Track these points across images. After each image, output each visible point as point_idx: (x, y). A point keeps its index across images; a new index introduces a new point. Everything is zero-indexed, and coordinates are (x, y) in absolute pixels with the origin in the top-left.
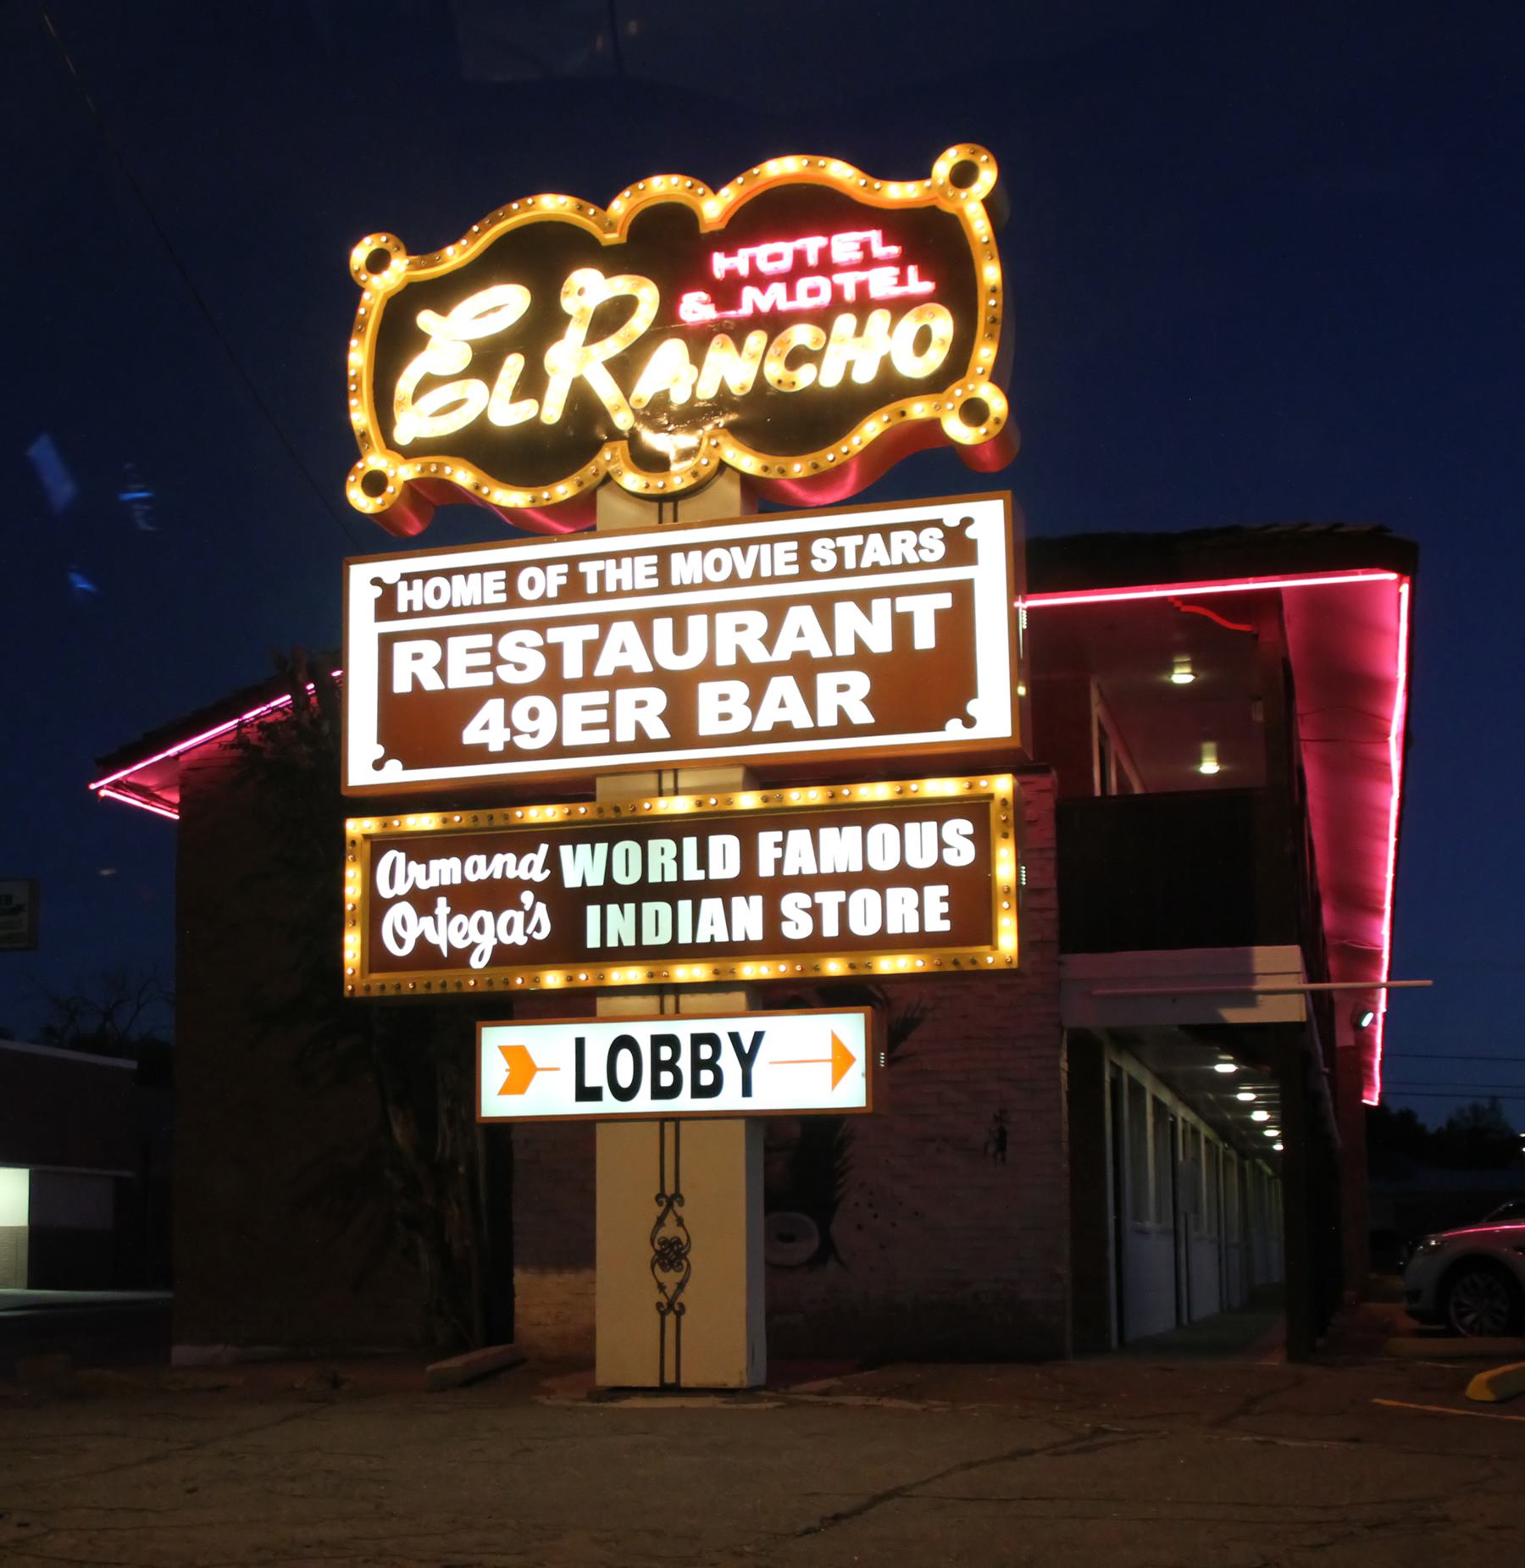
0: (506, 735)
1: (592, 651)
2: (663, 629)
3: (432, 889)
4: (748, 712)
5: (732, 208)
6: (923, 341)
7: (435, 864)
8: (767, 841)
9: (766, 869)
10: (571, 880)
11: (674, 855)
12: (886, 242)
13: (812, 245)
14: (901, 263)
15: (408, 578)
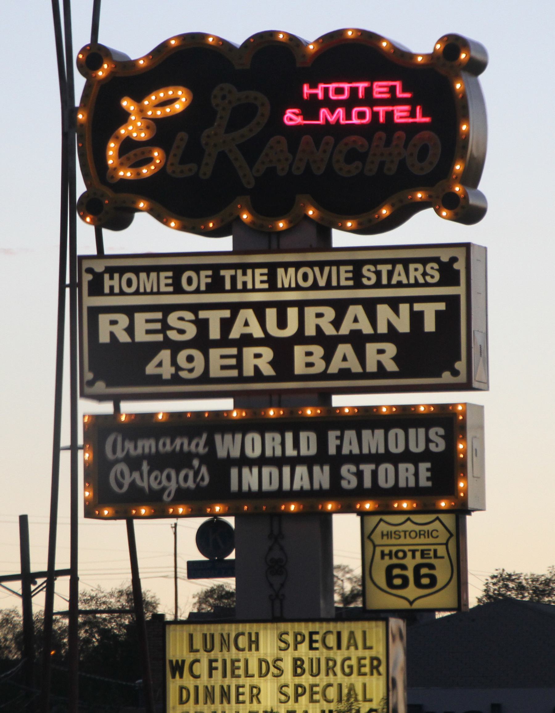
0: (173, 370)
2: (271, 314)
8: (332, 435)
9: (332, 451)
10: (221, 453)
12: (404, 90)
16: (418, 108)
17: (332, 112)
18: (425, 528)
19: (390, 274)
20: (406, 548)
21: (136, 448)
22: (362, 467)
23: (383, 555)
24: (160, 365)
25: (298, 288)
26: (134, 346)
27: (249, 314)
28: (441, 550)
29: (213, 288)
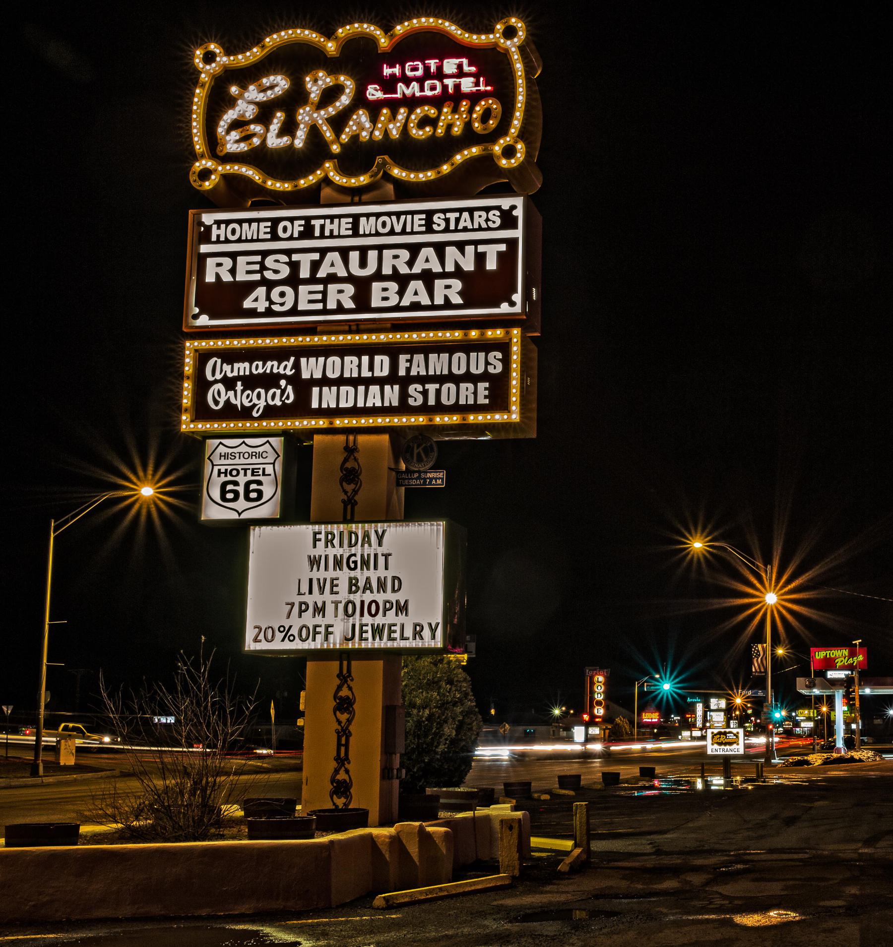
0: (267, 304)
1: (315, 266)
2: (354, 256)
3: (234, 377)
4: (397, 297)
5: (422, 29)
6: (486, 115)
7: (236, 365)
8: (403, 358)
9: (402, 372)
10: (305, 375)
11: (473, 391)
12: (470, 65)
13: (433, 64)
14: (476, 76)
15: (218, 223)
16: (482, 79)
17: (408, 87)
18: (257, 450)
19: (458, 220)
20: (239, 468)
21: (232, 371)
22: (427, 386)
23: (220, 473)
24: (256, 300)
25: (378, 234)
26: (235, 284)
27: (335, 256)
28: (269, 469)
29: (304, 235)
